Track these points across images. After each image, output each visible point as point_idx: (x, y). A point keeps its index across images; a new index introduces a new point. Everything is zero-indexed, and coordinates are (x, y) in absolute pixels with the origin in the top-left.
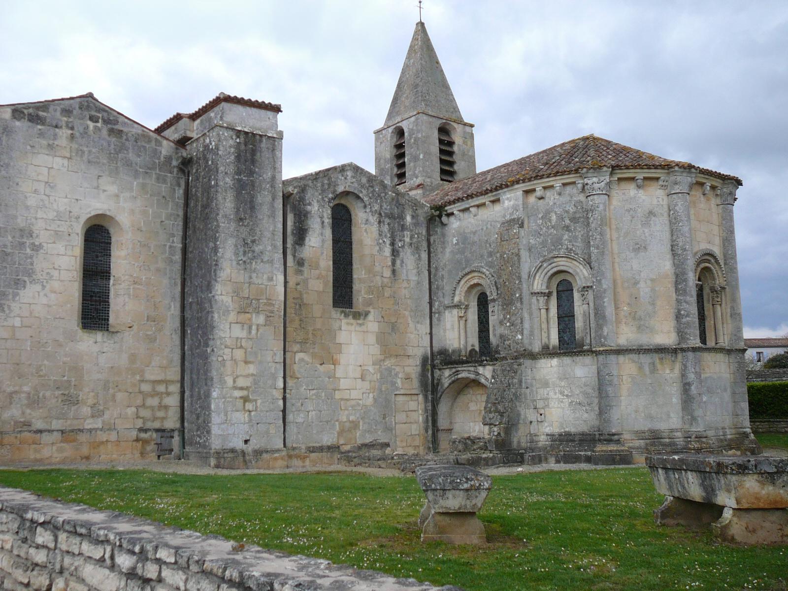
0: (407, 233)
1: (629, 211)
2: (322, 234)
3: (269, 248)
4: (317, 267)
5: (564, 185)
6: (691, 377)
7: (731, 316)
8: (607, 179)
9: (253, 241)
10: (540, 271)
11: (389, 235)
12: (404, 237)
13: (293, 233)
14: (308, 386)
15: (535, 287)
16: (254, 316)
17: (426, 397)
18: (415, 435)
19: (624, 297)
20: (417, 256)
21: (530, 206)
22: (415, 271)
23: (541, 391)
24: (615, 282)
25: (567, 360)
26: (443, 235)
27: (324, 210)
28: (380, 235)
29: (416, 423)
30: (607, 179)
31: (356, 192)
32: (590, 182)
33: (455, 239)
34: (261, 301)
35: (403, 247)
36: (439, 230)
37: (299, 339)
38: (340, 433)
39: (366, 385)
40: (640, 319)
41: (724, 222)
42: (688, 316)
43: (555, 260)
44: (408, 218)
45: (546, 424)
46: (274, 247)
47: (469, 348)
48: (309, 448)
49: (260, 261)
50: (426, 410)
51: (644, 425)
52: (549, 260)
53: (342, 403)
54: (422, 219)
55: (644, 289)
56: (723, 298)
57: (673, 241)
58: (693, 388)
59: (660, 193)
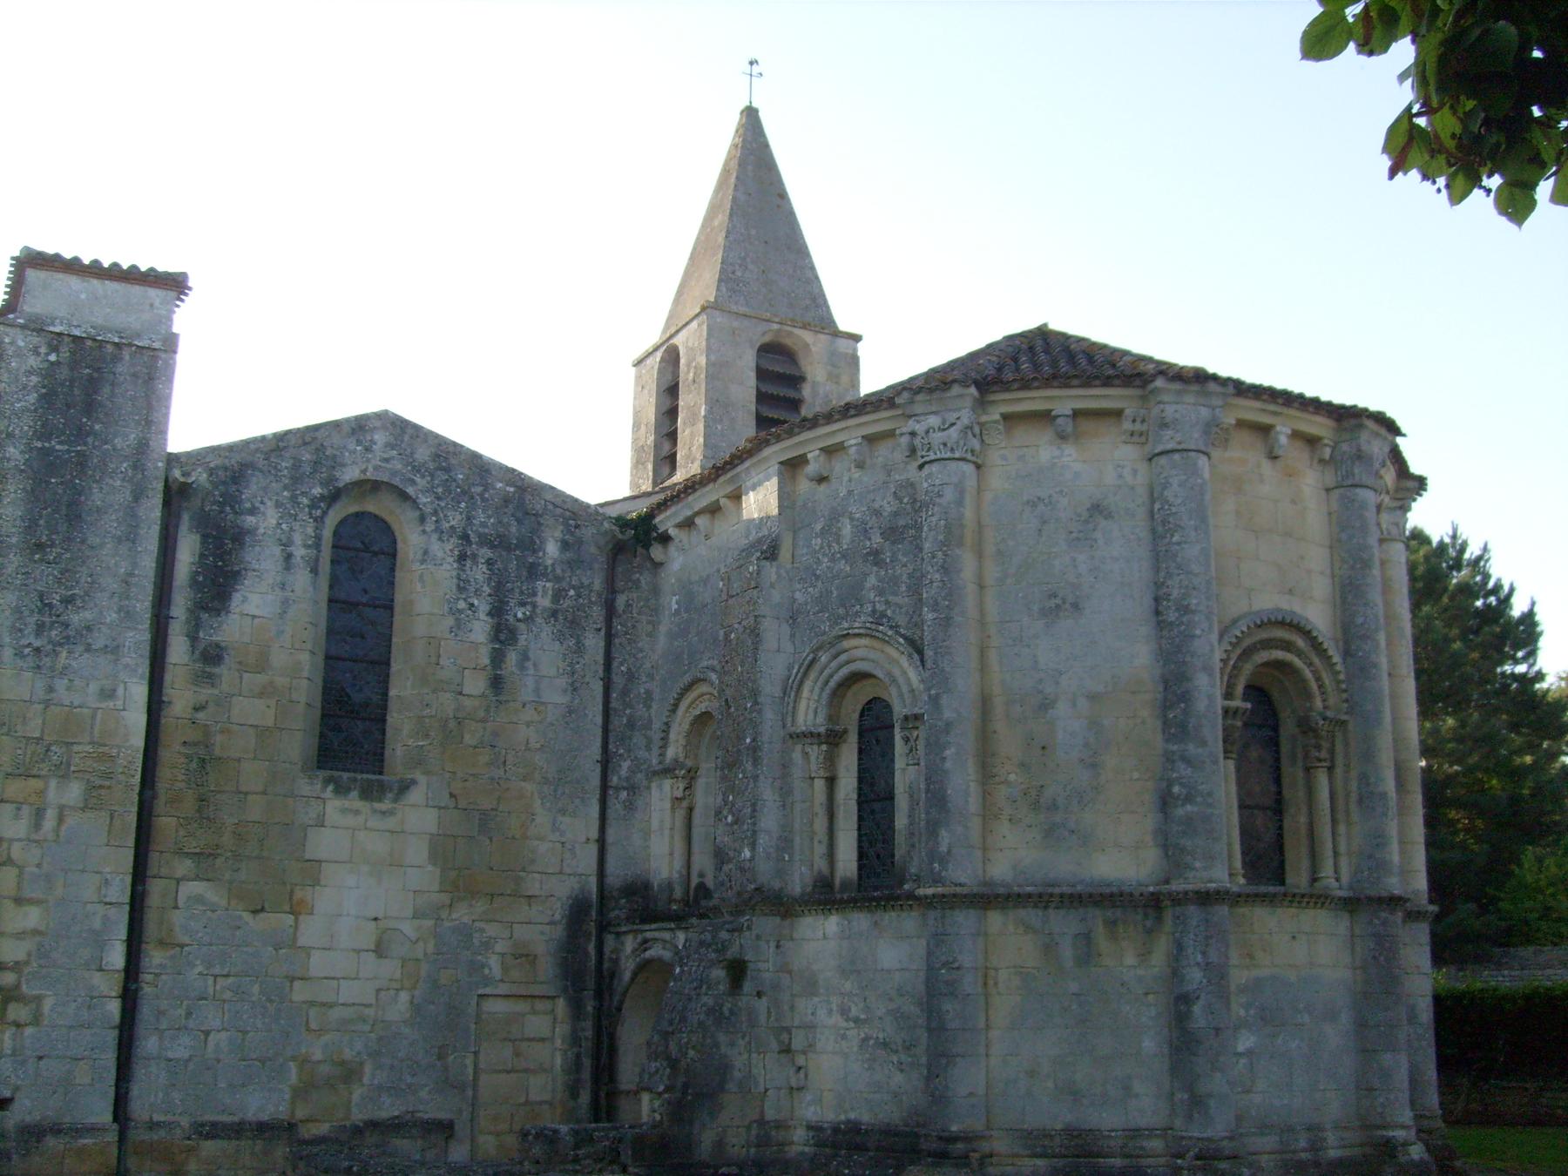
0: (545, 588)
1: (1034, 505)
2: (283, 587)
3: (111, 617)
4: (262, 665)
5: (871, 440)
6: (1195, 976)
7: (1360, 801)
8: (966, 417)
9: (68, 601)
10: (813, 675)
11: (487, 590)
12: (535, 594)
13: (194, 583)
14: (209, 965)
15: (800, 719)
16: (53, 783)
17: (576, 1007)
18: (541, 1103)
19: (1008, 743)
20: (572, 642)
21: (800, 503)
22: (562, 682)
23: (802, 1004)
24: (985, 704)
25: (861, 920)
26: (656, 591)
27: (296, 526)
28: (460, 589)
29: (545, 1070)
30: (966, 417)
31: (396, 481)
32: (920, 428)
33: (675, 599)
34: (76, 748)
35: (528, 620)
36: (645, 579)
37: (192, 846)
38: (299, 1093)
39: (390, 969)
40: (1053, 807)
41: (1344, 536)
42: (1188, 799)
43: (846, 644)
44: (552, 549)
45: (809, 1097)
46: (127, 614)
47: (695, 881)
48: (202, 1125)
49: (81, 648)
50: (575, 1040)
51: (1053, 1114)
52: (832, 645)
53: (313, 1012)
54: (593, 550)
55: (1068, 723)
56: (1339, 747)
57: (1158, 585)
58: (1197, 1009)
59: (1128, 454)
